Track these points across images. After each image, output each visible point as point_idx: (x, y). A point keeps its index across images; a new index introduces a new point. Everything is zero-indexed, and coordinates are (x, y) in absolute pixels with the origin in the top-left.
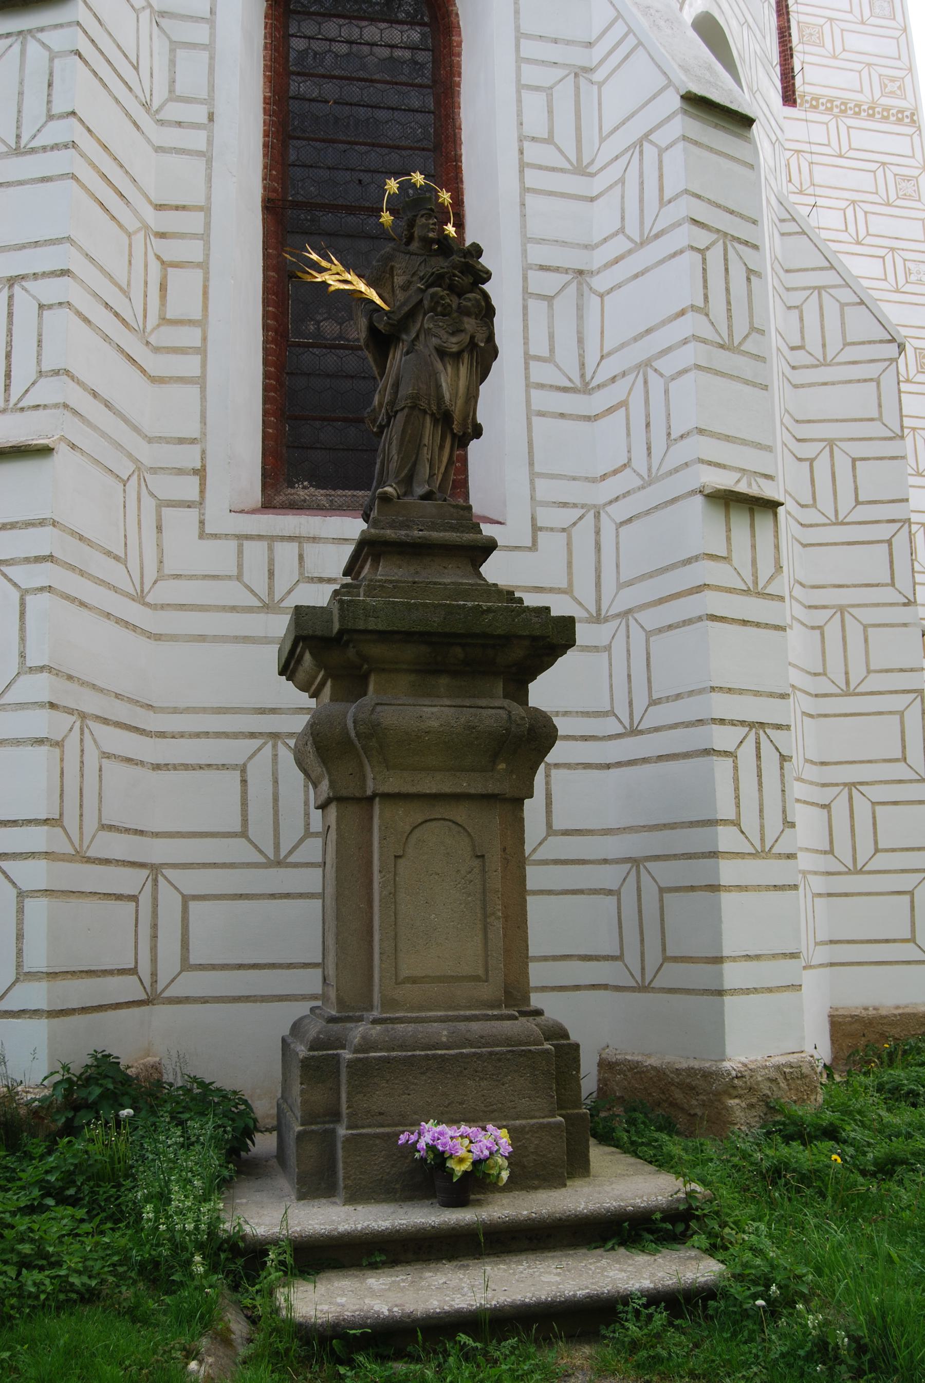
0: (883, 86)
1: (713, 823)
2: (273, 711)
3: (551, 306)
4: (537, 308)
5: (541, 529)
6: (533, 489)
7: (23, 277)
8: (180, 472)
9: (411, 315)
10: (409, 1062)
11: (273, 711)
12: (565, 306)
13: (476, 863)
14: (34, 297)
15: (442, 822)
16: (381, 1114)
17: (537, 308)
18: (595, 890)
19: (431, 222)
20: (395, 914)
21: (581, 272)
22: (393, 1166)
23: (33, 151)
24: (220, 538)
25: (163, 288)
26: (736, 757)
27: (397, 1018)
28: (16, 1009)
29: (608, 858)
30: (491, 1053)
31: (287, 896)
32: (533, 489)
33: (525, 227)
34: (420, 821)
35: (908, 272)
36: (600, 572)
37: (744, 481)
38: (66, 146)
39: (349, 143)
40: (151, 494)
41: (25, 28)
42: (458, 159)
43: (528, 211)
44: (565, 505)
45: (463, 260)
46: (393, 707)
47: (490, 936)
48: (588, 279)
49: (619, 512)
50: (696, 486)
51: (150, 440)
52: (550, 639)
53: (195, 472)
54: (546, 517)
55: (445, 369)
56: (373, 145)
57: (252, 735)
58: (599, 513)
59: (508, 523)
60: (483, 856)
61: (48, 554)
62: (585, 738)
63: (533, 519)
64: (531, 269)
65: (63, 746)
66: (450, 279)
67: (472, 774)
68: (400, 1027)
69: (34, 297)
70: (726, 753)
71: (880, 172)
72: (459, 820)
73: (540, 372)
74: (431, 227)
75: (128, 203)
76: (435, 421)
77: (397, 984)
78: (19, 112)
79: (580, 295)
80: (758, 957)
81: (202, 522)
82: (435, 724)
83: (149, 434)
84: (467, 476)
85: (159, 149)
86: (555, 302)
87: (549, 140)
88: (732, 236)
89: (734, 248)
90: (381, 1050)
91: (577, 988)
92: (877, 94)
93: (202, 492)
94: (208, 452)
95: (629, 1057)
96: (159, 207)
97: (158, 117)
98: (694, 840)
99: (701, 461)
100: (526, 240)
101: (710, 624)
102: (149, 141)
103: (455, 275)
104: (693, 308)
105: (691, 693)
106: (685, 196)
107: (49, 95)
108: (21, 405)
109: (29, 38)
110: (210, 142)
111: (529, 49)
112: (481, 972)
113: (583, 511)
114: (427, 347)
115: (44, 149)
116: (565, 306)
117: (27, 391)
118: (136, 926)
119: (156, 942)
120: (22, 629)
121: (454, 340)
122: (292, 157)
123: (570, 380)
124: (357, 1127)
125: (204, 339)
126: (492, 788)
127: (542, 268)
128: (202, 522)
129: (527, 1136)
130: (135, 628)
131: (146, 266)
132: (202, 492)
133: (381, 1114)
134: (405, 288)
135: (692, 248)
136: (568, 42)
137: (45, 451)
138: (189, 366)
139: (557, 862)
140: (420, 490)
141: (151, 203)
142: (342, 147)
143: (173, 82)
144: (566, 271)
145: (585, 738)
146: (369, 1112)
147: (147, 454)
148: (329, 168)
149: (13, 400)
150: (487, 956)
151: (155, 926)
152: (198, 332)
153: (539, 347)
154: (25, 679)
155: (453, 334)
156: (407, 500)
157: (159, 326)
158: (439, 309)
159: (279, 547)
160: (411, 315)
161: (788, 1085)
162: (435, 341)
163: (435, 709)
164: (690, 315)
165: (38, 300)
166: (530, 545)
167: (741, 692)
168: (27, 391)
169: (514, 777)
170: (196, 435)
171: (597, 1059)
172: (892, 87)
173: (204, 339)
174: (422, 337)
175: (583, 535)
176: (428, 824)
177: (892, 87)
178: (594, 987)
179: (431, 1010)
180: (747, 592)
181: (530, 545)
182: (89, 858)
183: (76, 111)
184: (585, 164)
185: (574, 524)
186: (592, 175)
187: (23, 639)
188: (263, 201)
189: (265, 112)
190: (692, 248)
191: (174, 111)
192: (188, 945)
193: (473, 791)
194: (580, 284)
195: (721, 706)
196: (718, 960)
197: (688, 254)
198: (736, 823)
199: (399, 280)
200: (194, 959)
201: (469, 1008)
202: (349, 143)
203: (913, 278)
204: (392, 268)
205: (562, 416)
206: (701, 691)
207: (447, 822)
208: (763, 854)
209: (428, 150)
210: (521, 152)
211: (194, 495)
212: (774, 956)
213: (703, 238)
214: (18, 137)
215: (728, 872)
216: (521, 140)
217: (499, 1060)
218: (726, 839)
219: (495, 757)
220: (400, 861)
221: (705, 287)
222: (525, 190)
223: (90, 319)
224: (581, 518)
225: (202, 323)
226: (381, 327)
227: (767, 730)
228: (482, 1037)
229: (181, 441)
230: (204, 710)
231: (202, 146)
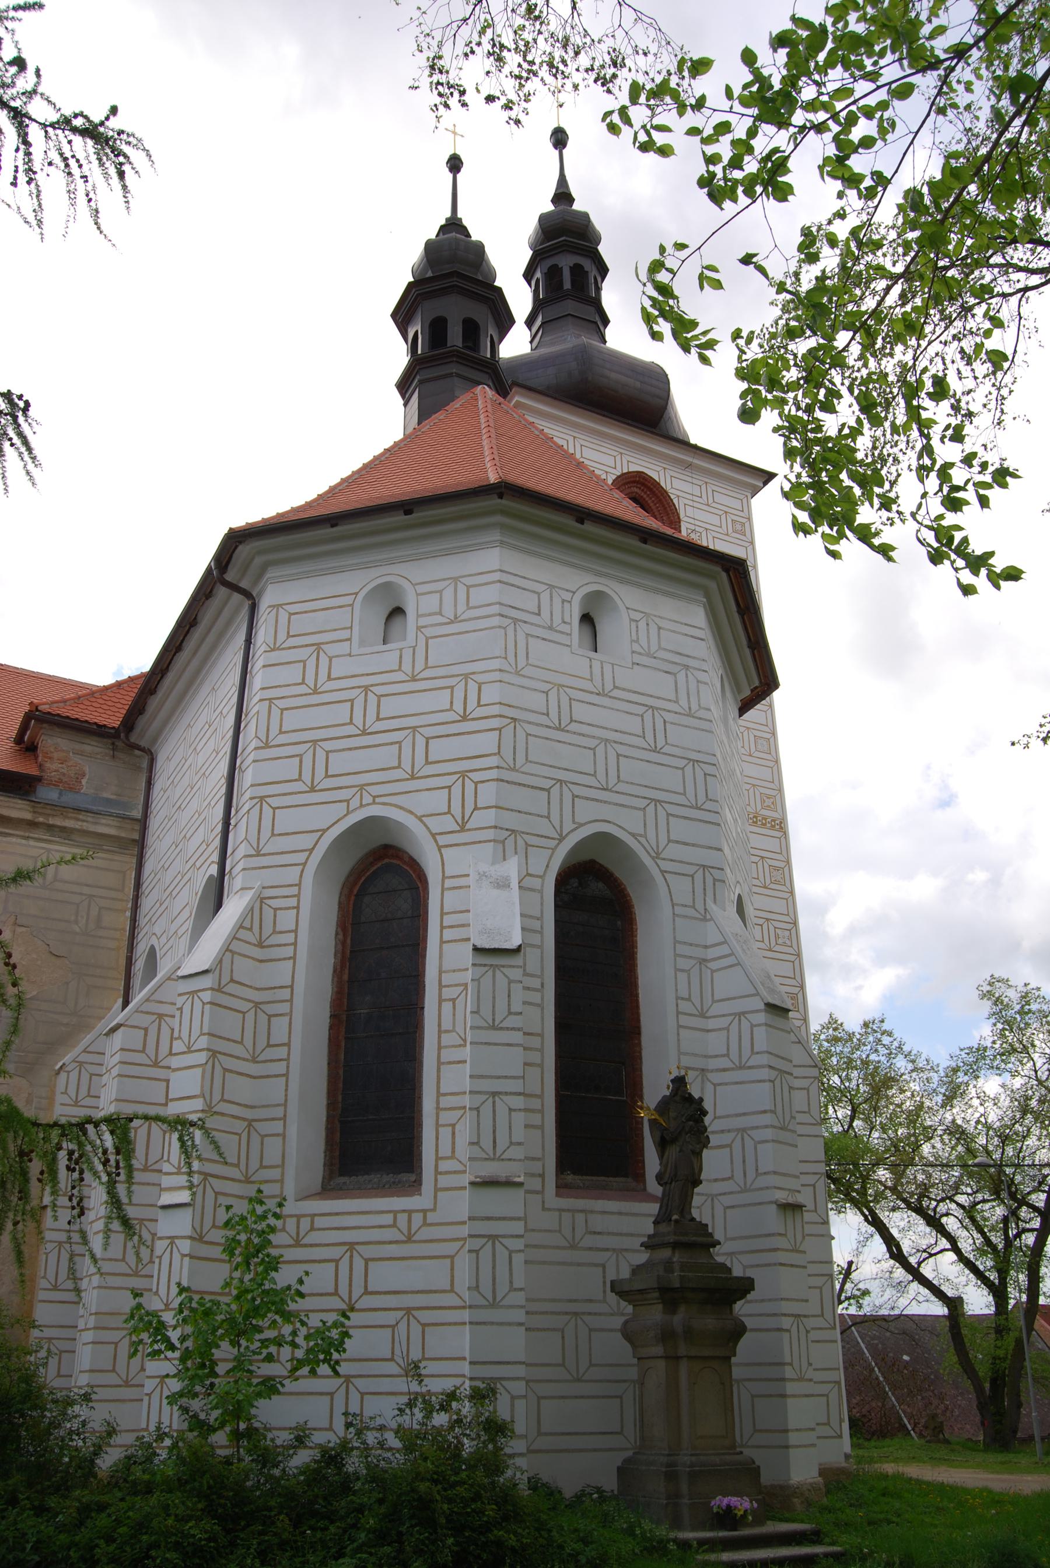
0: (763, 801)
2: (575, 1301)
7: (500, 1093)
11: (575, 1301)
23: (501, 1029)
31: (582, 1397)
35: (777, 937)
42: (637, 995)
52: (745, 1286)
53: (540, 1175)
57: (567, 1313)
71: (760, 864)
79: (703, 1081)
87: (689, 999)
92: (759, 807)
100: (680, 1053)
105: (770, 1300)
111: (682, 949)
115: (507, 1029)
120: (511, 1270)
136: (697, 946)
154: (512, 1294)
159: (577, 1215)
172: (768, 802)
177: (768, 802)
180: (792, 1251)
187: (511, 1274)
196: (786, 1431)
199: (672, 1114)
200: (543, 1430)
203: (780, 941)
211: (539, 1188)
215: (790, 1388)
218: (789, 1372)
222: (679, 1026)
230: (545, 1300)
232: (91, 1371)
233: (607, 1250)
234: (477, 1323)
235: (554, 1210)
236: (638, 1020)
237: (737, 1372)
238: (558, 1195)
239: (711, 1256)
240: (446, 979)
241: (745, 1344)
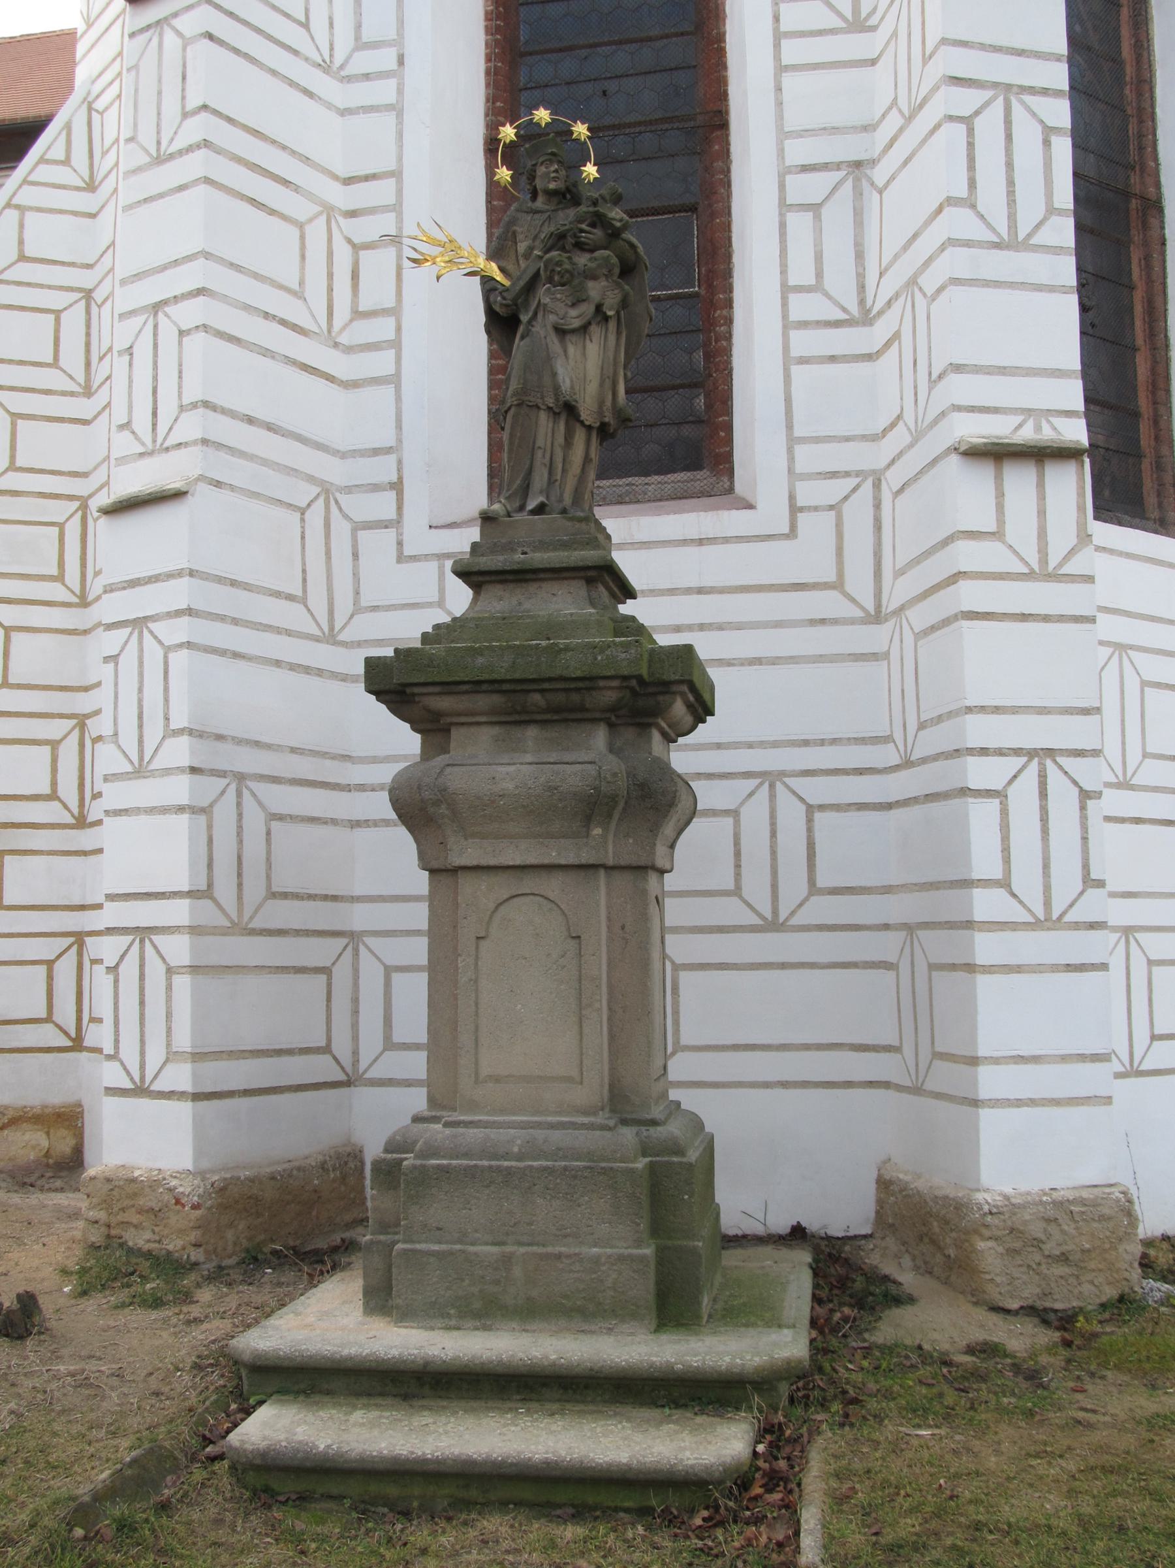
1: (967, 884)
3: (818, 218)
4: (799, 223)
5: (801, 509)
6: (791, 459)
7: (165, 302)
8: (375, 488)
9: (531, 286)
10: (471, 1173)
12: (838, 214)
13: (573, 943)
14: (175, 323)
15: (532, 897)
16: (439, 1229)
17: (799, 223)
18: (873, 962)
19: (552, 169)
20: (477, 1004)
21: (858, 164)
22: (448, 1288)
24: (419, 560)
25: (355, 276)
26: (1006, 796)
27: (471, 1122)
28: (167, 1089)
29: (891, 922)
30: (565, 1168)
32: (791, 459)
33: (782, 119)
34: (505, 897)
36: (880, 557)
37: (1030, 424)
38: (199, 147)
39: (591, 46)
40: (346, 517)
41: (161, 16)
42: (721, 38)
43: (786, 96)
44: (833, 475)
45: (591, 209)
46: (464, 769)
47: (586, 1030)
48: (868, 172)
49: (894, 479)
50: (949, 443)
51: (343, 455)
54: (807, 493)
55: (565, 351)
56: (620, 42)
58: (880, 480)
59: (760, 505)
60: (579, 937)
61: (185, 607)
62: (860, 772)
63: (792, 497)
64: (790, 173)
65: (212, 812)
66: (575, 236)
67: (562, 841)
68: (472, 1131)
69: (175, 323)
70: (989, 793)
72: (551, 896)
73: (804, 307)
74: (553, 175)
75: (297, 189)
76: (554, 413)
77: (476, 1082)
78: (159, 114)
79: (858, 194)
80: (1035, 1059)
81: (400, 544)
82: (509, 786)
83: (342, 448)
84: (732, 449)
85: (344, 112)
86: (824, 211)
88: (1020, 87)
89: (1023, 103)
90: (444, 1157)
91: (848, 1084)
93: (400, 508)
94: (405, 461)
95: (901, 1176)
96: (348, 181)
97: (343, 73)
98: (945, 905)
99: (958, 408)
101: (965, 624)
102: (329, 106)
103: (582, 231)
104: (951, 201)
106: (943, 47)
107: (183, 90)
108: (165, 445)
109: (165, 27)
110: (400, 91)
112: (575, 1073)
113: (858, 480)
114: (542, 329)
116: (838, 214)
117: (171, 429)
118: (329, 999)
119: (358, 1017)
121: (573, 313)
122: (523, 81)
123: (844, 310)
124: (412, 1242)
125: (399, 329)
126: (586, 857)
127: (805, 169)
128: (400, 544)
129: (604, 1268)
130: (320, 673)
131: (330, 254)
132: (400, 508)
133: (439, 1229)
134: (527, 256)
135: (951, 118)
137: (178, 495)
138: (383, 363)
139: (821, 928)
140: (531, 505)
141: (336, 177)
142: (584, 52)
143: (358, 27)
144: (838, 166)
145: (860, 772)
146: (426, 1225)
147: (335, 471)
148: (568, 84)
149: (160, 440)
150: (582, 1054)
151: (355, 1001)
152: (391, 322)
153: (801, 273)
155: (573, 305)
156: (518, 517)
157: (351, 321)
158: (556, 278)
160: (531, 286)
161: (1077, 1229)
162: (552, 318)
163: (512, 769)
164: (947, 210)
165: (178, 326)
166: (786, 530)
167: (1015, 710)
168: (171, 429)
169: (631, 841)
170: (392, 443)
171: (875, 1176)
173: (399, 329)
174: (540, 316)
175: (858, 514)
176: (515, 900)
178: (871, 1084)
179: (514, 1114)
181: (786, 530)
182: (253, 930)
183: (208, 103)
184: (863, 15)
185: (846, 498)
186: (873, 29)
188: (485, 143)
189: (488, 31)
190: (951, 118)
191: (365, 62)
192: (391, 1021)
193: (563, 862)
194: (857, 180)
195: (978, 730)
197: (947, 127)
198: (1005, 883)
199: (522, 247)
201: (559, 1113)
202: (591, 46)
204: (514, 233)
205: (833, 359)
206: (951, 714)
207: (538, 898)
208: (1048, 924)
209: (688, 33)
210: (777, 19)
211: (392, 514)
212: (1064, 1058)
213: (966, 100)
214: (159, 143)
215: (986, 948)
216: (777, 4)
217: (575, 1177)
219: (588, 820)
220: (484, 944)
221: (971, 167)
223: (240, 336)
224: (854, 490)
225: (395, 312)
226: (497, 308)
227: (1058, 759)
228: (559, 1149)
229: (376, 452)
231: (391, 98)
235: (426, 557)
236: (723, 96)
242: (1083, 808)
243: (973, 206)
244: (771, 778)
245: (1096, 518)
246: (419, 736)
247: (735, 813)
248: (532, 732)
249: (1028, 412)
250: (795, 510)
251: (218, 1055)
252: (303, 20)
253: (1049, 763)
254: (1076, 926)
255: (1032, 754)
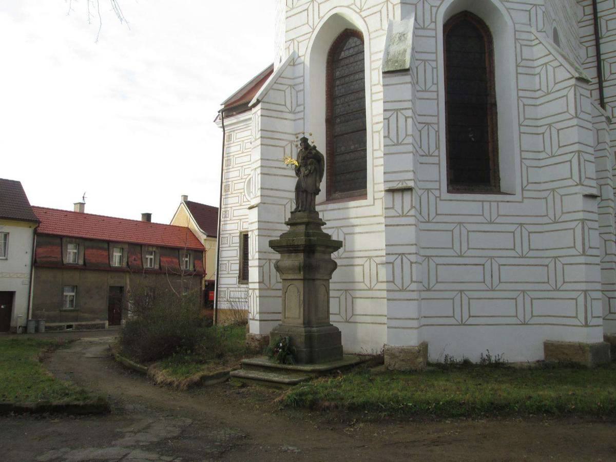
52: (337, 245)
63: (374, 197)
143: (297, 102)
210: (371, 90)
232: (387, 282)
233: (333, 228)
234: (264, 320)
237: (332, 286)
238: (449, 192)
239: (320, 230)
240: (486, 205)
241: (335, 275)
242: (411, 265)
243: (389, 137)
244: (370, 258)
245: (449, 192)
246: (280, 255)
247: (363, 265)
248: (293, 254)
249: (400, 181)
250: (374, 199)
251: (265, 313)
252: (509, 10)
253: (403, 256)
254: (409, 291)
255: (399, 254)
